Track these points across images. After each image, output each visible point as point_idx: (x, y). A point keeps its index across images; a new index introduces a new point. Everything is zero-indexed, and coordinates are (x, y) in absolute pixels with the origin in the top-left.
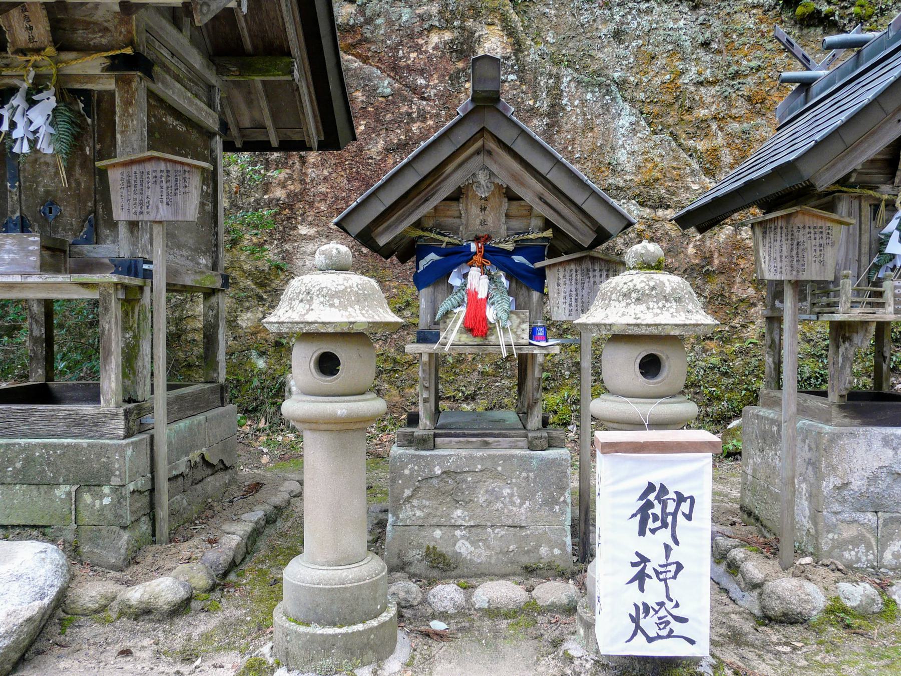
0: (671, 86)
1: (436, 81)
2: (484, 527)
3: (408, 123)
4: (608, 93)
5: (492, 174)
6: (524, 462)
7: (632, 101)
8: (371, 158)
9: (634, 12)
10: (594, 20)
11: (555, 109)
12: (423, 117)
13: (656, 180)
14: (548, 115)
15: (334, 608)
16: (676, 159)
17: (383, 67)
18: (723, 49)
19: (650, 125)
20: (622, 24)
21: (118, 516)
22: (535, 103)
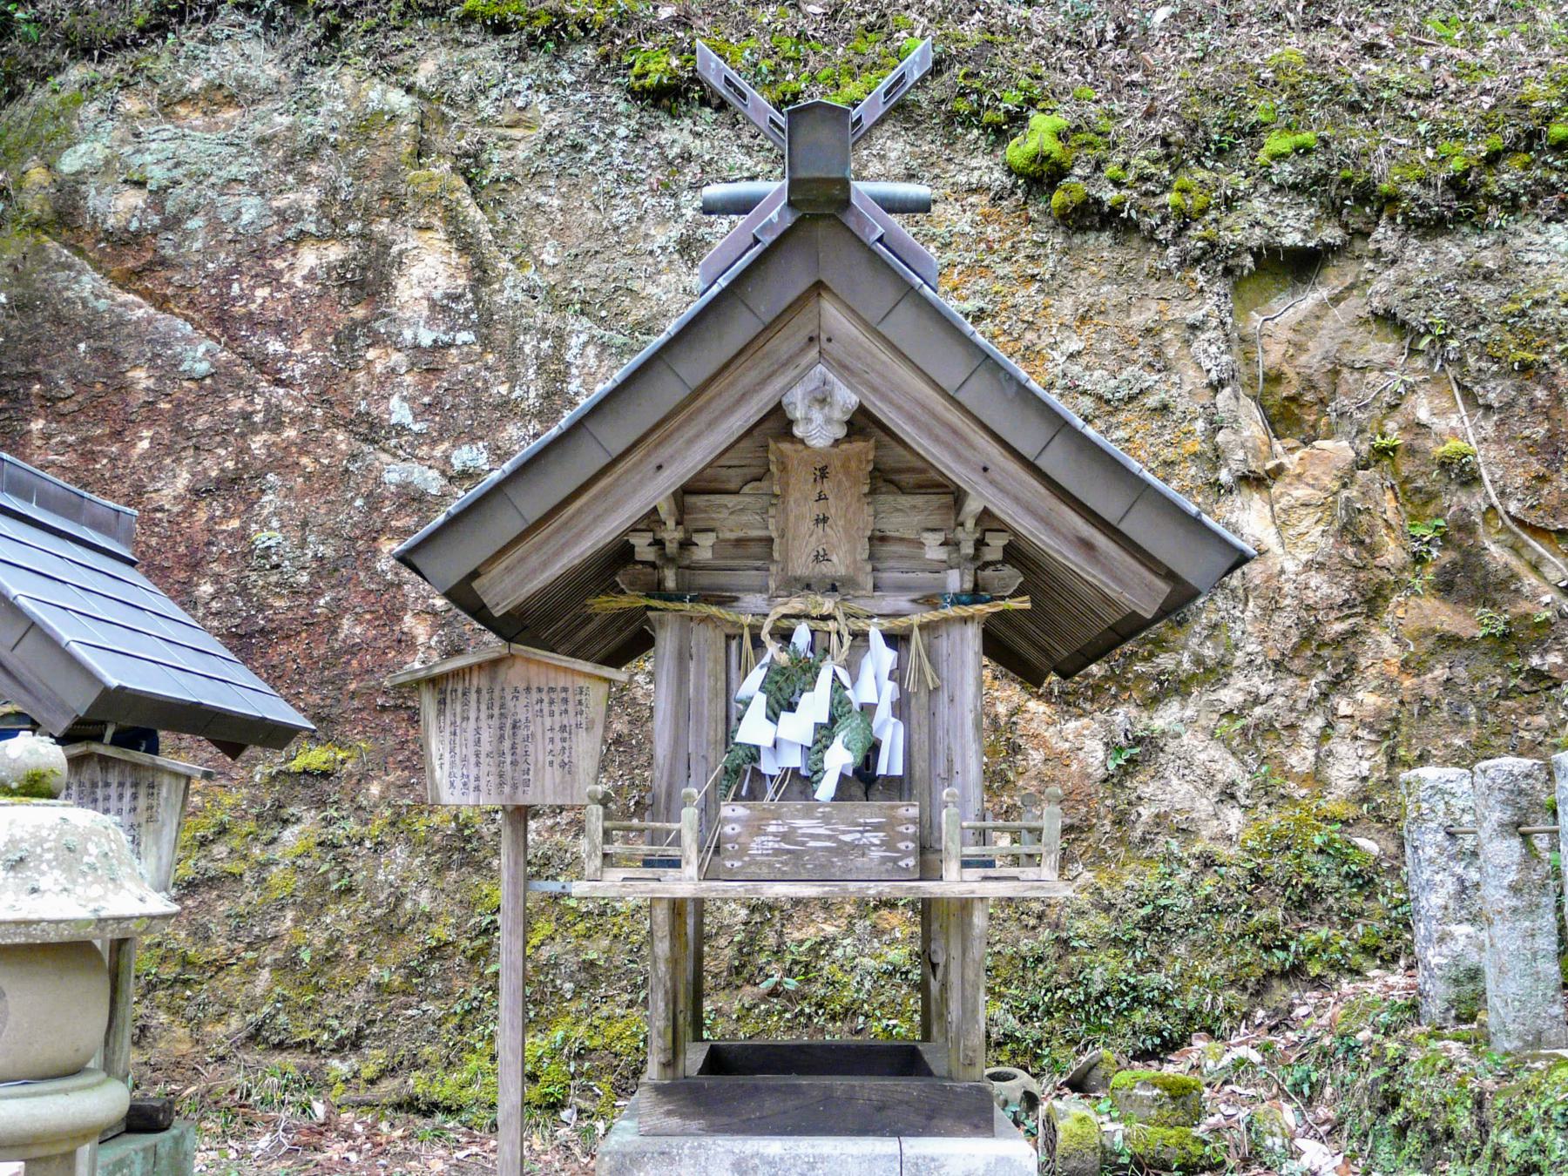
1: (307, 347)
3: (243, 435)
8: (161, 509)
10: (640, 219)
12: (275, 421)
14: (539, 415)
17: (197, 317)
20: (698, 226)
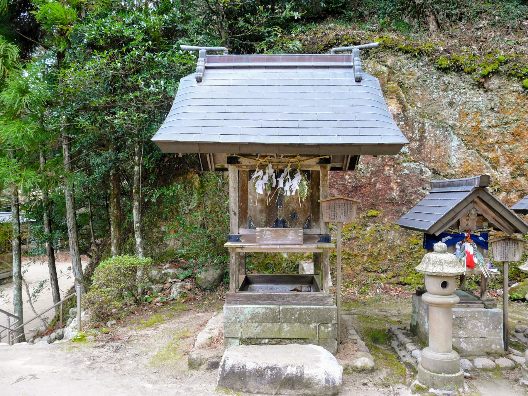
0: (476, 128)
2: (471, 337)
4: (447, 131)
5: (477, 210)
6: (485, 314)
7: (458, 135)
9: (458, 93)
10: (440, 97)
11: (422, 138)
13: (469, 171)
15: (450, 368)
16: (479, 161)
18: (500, 111)
19: (466, 145)
21: (334, 335)
22: (413, 135)
